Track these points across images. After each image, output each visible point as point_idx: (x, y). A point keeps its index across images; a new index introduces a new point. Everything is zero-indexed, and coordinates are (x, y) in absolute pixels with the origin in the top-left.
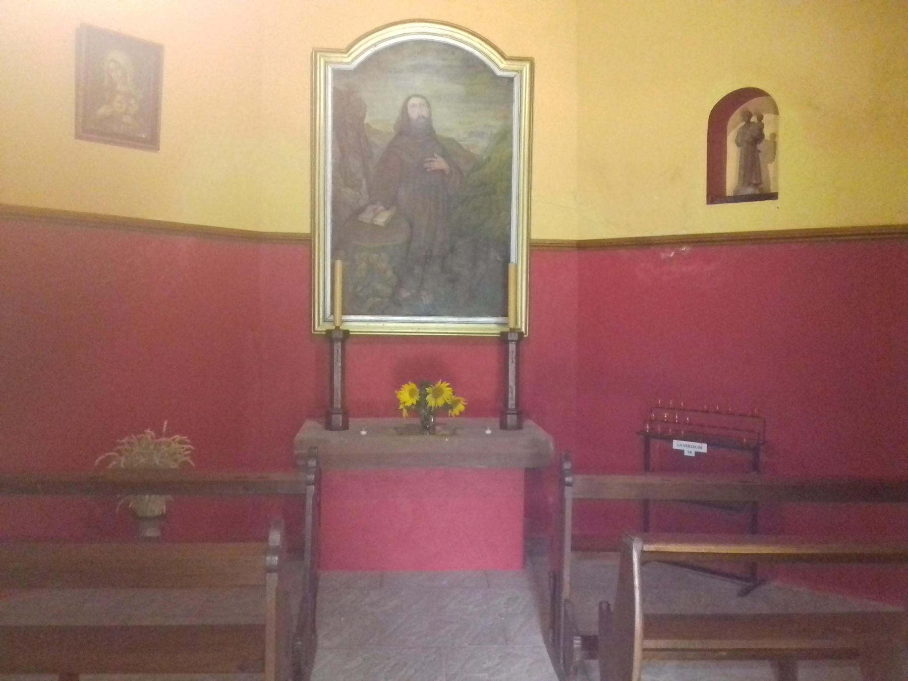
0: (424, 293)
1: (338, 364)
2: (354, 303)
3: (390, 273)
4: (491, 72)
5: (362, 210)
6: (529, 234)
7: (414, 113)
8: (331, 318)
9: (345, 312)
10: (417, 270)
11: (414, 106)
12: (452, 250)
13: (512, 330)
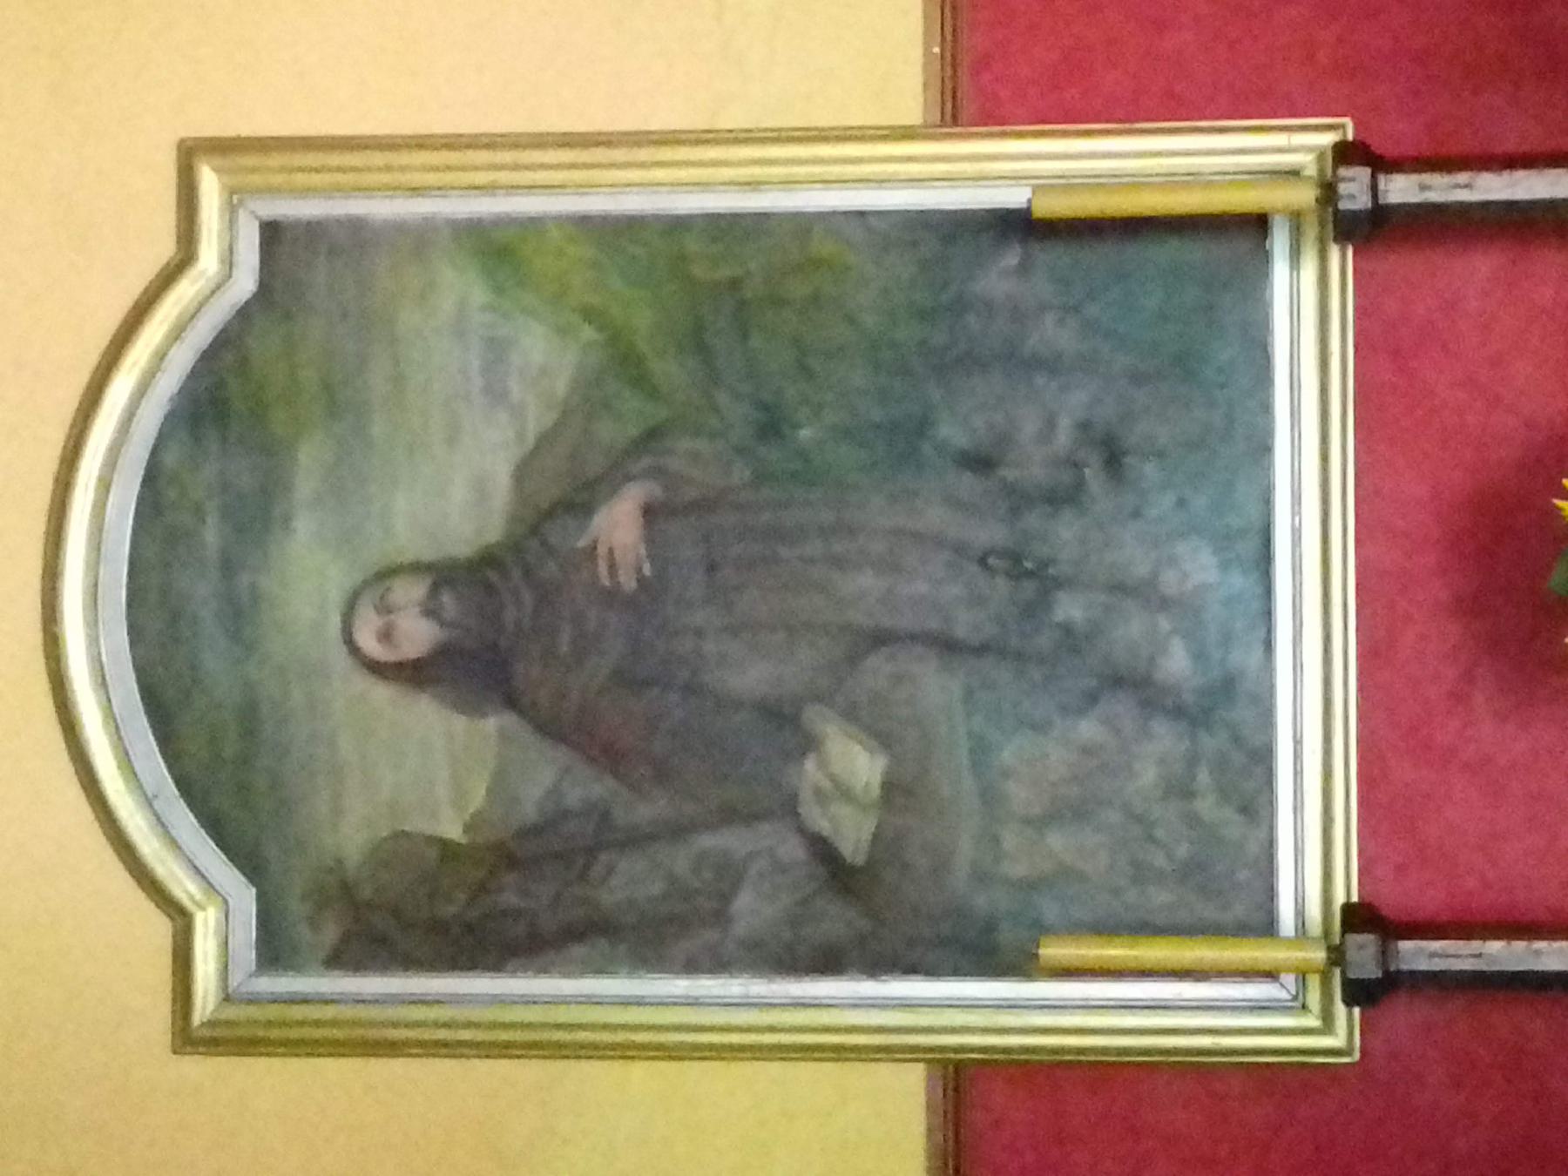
0: (1169, 581)
1: (1500, 954)
2: (1222, 897)
3: (1088, 729)
4: (244, 313)
5: (823, 851)
6: (906, 134)
7: (417, 635)
8: (1289, 979)
9: (1267, 927)
10: (1070, 608)
11: (386, 636)
12: (980, 462)
13: (1337, 956)
